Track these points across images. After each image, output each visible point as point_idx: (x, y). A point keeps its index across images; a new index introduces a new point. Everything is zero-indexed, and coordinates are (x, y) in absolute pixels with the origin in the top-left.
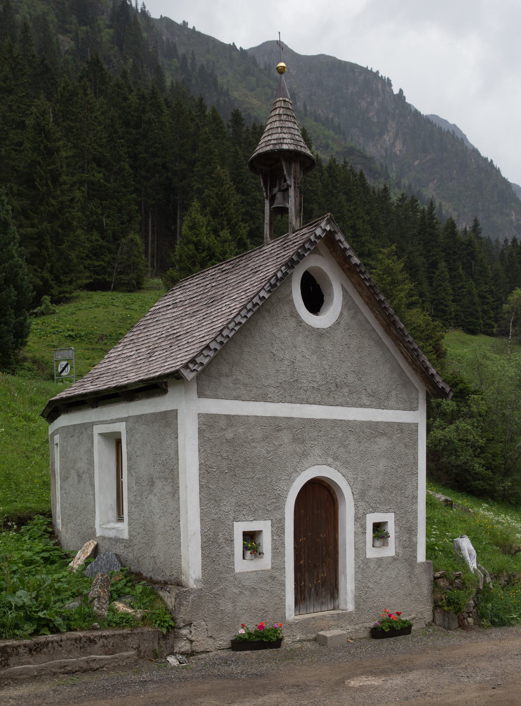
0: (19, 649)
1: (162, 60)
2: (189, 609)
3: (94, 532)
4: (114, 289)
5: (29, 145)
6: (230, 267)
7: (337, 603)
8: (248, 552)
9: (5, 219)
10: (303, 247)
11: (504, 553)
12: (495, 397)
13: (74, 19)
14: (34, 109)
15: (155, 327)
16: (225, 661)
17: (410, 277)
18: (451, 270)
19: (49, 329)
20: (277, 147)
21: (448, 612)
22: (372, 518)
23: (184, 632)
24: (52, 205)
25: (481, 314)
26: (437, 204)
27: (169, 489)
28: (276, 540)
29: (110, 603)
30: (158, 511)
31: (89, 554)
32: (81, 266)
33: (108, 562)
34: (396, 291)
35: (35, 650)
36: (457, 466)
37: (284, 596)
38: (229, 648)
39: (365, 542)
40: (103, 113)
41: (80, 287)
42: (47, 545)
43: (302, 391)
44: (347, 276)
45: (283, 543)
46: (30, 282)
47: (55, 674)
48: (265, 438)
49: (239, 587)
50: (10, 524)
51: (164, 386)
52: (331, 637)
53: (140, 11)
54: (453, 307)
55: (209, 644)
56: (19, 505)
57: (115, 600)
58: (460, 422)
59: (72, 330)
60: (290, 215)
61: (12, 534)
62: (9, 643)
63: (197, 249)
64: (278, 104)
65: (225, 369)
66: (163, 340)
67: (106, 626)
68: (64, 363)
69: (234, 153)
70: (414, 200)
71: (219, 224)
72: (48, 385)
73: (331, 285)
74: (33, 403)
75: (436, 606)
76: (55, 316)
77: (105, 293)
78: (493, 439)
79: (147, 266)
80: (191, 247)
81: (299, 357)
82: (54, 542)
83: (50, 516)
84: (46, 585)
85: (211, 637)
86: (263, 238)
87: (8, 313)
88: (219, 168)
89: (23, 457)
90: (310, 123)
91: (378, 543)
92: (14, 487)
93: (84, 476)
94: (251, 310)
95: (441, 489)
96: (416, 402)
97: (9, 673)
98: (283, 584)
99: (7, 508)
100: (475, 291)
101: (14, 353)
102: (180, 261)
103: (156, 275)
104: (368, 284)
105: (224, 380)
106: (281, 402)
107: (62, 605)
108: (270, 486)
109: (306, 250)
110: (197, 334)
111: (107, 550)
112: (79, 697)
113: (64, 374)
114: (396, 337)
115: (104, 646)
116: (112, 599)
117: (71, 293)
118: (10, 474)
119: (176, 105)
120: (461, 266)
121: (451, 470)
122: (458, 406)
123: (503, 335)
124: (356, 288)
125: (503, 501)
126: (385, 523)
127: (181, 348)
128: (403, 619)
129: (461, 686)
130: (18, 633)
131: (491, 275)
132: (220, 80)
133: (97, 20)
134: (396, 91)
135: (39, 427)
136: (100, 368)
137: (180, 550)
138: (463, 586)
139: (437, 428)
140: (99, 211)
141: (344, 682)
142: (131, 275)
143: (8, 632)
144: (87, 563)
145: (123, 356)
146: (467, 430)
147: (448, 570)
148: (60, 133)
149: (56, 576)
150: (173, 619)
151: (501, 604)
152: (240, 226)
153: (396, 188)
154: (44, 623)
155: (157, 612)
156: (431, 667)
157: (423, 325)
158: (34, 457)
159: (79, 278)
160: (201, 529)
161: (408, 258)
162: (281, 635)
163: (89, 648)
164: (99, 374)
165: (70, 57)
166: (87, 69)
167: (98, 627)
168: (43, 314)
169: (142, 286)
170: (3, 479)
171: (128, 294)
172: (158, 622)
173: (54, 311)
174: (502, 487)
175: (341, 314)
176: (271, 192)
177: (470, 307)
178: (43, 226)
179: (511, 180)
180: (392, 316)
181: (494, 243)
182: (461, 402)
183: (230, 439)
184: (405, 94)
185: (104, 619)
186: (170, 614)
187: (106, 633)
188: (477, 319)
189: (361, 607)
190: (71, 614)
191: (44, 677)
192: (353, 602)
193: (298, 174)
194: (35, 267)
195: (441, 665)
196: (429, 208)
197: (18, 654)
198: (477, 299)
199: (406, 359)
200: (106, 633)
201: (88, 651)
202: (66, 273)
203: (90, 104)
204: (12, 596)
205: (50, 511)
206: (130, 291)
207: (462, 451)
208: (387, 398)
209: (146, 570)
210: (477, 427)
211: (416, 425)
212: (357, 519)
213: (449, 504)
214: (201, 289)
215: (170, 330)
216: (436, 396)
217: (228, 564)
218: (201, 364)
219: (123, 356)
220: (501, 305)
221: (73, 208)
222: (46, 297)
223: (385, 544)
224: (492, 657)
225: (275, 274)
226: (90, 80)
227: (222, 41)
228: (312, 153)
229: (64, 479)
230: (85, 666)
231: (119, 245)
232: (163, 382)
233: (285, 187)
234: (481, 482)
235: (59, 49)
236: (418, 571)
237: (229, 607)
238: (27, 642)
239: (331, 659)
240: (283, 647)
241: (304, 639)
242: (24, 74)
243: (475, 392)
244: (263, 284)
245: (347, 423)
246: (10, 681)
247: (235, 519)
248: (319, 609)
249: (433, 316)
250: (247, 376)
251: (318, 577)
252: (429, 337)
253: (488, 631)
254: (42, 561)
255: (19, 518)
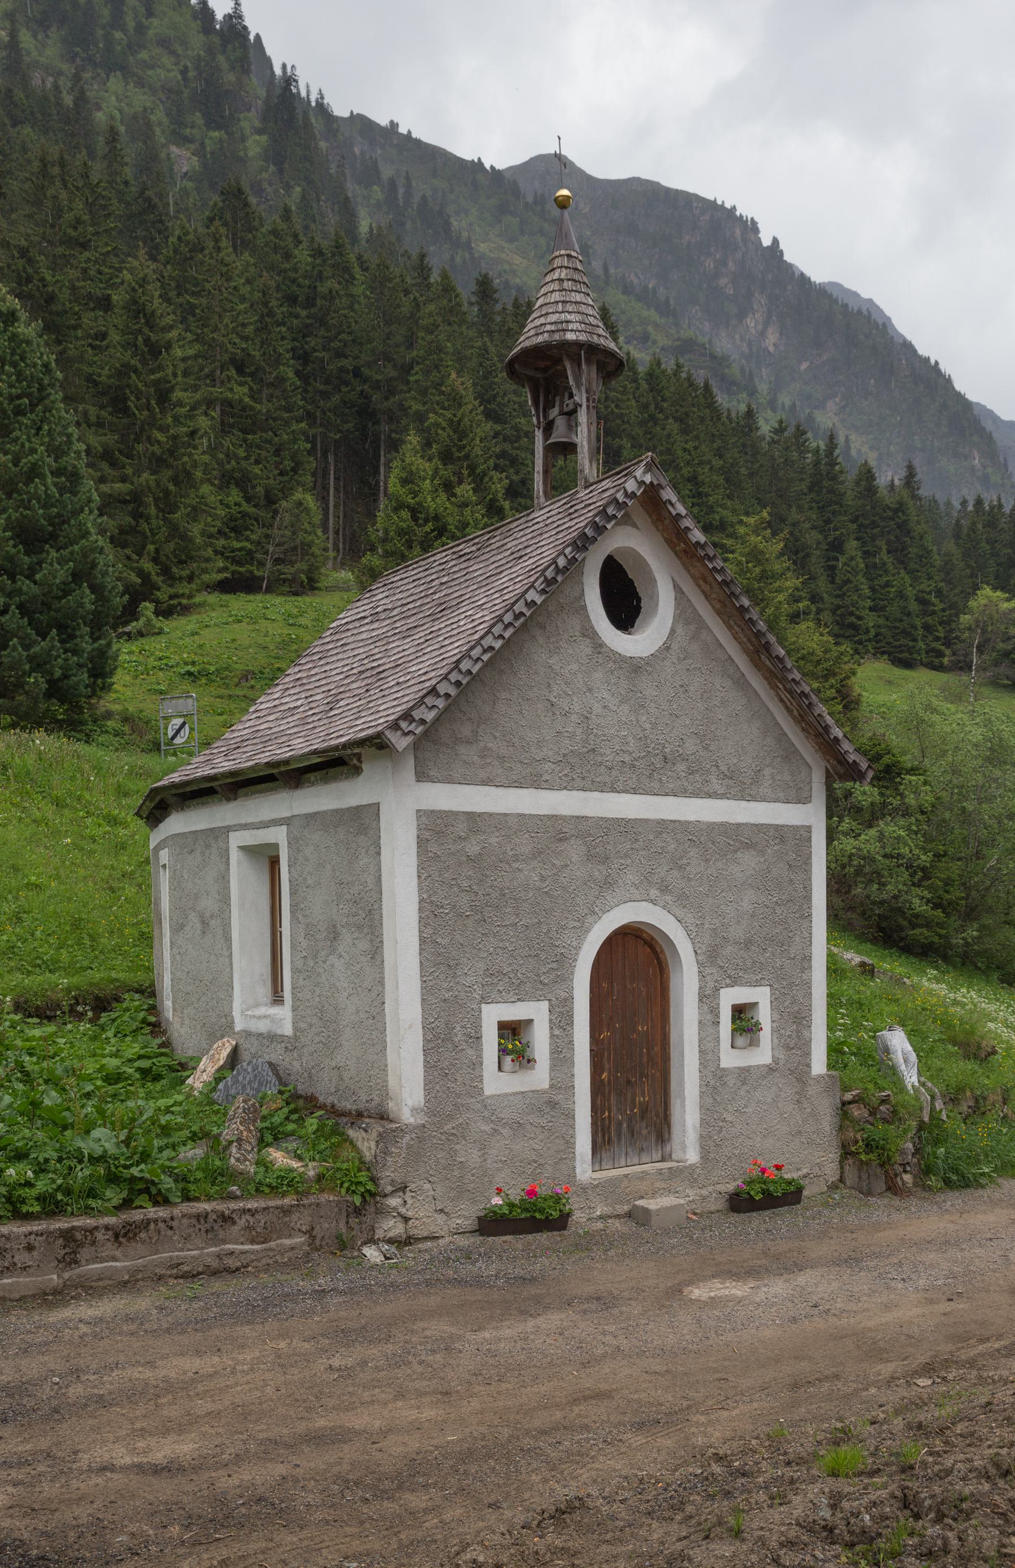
0: (96, 1234)
1: (352, 188)
2: (401, 1162)
3: (231, 1024)
4: (269, 590)
5: (118, 338)
6: (474, 548)
7: (668, 1149)
8: (509, 1058)
9: (75, 467)
10: (603, 512)
11: (967, 1057)
12: (948, 778)
13: (198, 118)
14: (126, 275)
15: (340, 656)
16: (468, 1255)
17: (793, 567)
18: (867, 554)
19: (152, 662)
20: (557, 337)
21: (867, 1163)
22: (730, 997)
23: (394, 1202)
24: (158, 442)
25: (921, 632)
26: (841, 439)
27: (364, 945)
28: (558, 1036)
29: (260, 1151)
30: (346, 985)
31: (221, 1062)
32: (210, 550)
33: (255, 1076)
34: (770, 592)
35: (125, 1235)
36: (882, 902)
37: (573, 1136)
38: (474, 1232)
39: (717, 1039)
40: (248, 281)
41: (208, 586)
42: (146, 1047)
43: (603, 769)
44: (683, 564)
45: (571, 1042)
46: (118, 579)
47: (160, 1278)
48: (536, 854)
49: (492, 1121)
50: (80, 1009)
51: (355, 761)
52: (658, 1210)
53: (313, 104)
54: (871, 620)
55: (438, 1224)
56: (97, 976)
57: (268, 1145)
58: (887, 824)
59: (193, 663)
60: (579, 457)
61: (84, 1026)
62: (78, 1222)
63: (415, 518)
64: (557, 262)
65: (466, 731)
66: (353, 678)
67: (253, 1192)
68: (178, 722)
69: (479, 348)
70: (800, 432)
71: (454, 474)
72: (149, 761)
73: (653, 581)
74: (122, 792)
75: (846, 1153)
76: (163, 639)
77: (251, 597)
78: (945, 855)
79: (326, 550)
80: (405, 514)
81: (597, 708)
82: (159, 1041)
83: (153, 994)
84: (144, 1118)
85: (441, 1211)
86: (532, 498)
87: (78, 633)
88: (453, 375)
89: (104, 889)
90: (615, 297)
91: (740, 1041)
92: (87, 942)
93: (213, 923)
94: (510, 624)
95: (853, 944)
96: (807, 788)
97: (79, 1276)
98: (570, 1116)
99: (75, 980)
100: (910, 592)
101: (89, 704)
102: (385, 540)
103: (343, 564)
104: (720, 579)
105: (462, 749)
106: (565, 788)
107: (173, 1154)
108: (547, 940)
109: (610, 518)
110: (414, 669)
111: (254, 1056)
112: (204, 1320)
113: (178, 741)
114: (771, 672)
115: (248, 1228)
116: (262, 1143)
117: (190, 597)
118: (80, 919)
119: (378, 266)
120: (884, 548)
121: (871, 909)
122: (881, 794)
123: (961, 669)
124: (699, 586)
125: (963, 964)
126: (754, 1005)
127: (386, 692)
128: (787, 1176)
129: (892, 1296)
130: (94, 1205)
131: (938, 563)
132: (455, 223)
133: (239, 120)
134: (767, 242)
135: (133, 836)
136: (241, 730)
137: (385, 1055)
138: (894, 1117)
139: (846, 834)
140: (241, 453)
141: (681, 1291)
142: (298, 565)
143: (77, 1202)
144: (218, 1080)
145: (282, 708)
146: (899, 838)
147: (866, 1089)
148: (172, 317)
149: (162, 1103)
150: (373, 1180)
151: (961, 1148)
152: (491, 478)
153: (769, 411)
154: (141, 1186)
155: (345, 1166)
156: (838, 1262)
157: (819, 652)
158: (124, 888)
159: (205, 571)
160: (423, 1016)
161: (791, 533)
162: (568, 1207)
163: (221, 1232)
164: (239, 739)
165: (190, 185)
166: (221, 204)
167: (238, 1193)
168: (141, 634)
169: (318, 585)
170: (68, 929)
171: (293, 598)
172: (346, 1185)
173: (161, 629)
174: (963, 939)
175: (673, 631)
176: (545, 416)
177: (901, 620)
178: (141, 479)
179: (972, 396)
180: (764, 634)
181: (942, 507)
182: (887, 788)
183: (475, 856)
184: (782, 246)
185: (250, 1180)
186: (368, 1169)
187: (252, 1205)
188: (915, 640)
189: (712, 1155)
190: (189, 1171)
191: (141, 1283)
192: (698, 1148)
193: (594, 384)
194: (128, 551)
195: (856, 1260)
196: (827, 446)
197: (93, 1243)
198: (914, 606)
199: (790, 711)
200: (252, 1205)
201: (221, 1236)
202: (181, 562)
203: (226, 265)
204: (83, 1139)
205: (152, 985)
206: (296, 594)
207: (891, 876)
208: (756, 781)
209: (325, 1090)
210: (916, 833)
211: (808, 829)
212: (702, 997)
213: (867, 970)
214: (422, 588)
215: (365, 661)
216: (843, 778)
217: (472, 1080)
218: (423, 722)
219: (282, 708)
220: (957, 615)
221: (195, 448)
222: (147, 604)
223: (754, 1043)
224: (946, 1243)
225: (554, 562)
226: (225, 224)
227: (458, 155)
228: (620, 349)
229: (178, 928)
230: (215, 1264)
231: (276, 512)
232: (355, 755)
233: (571, 407)
234: (924, 931)
235: (172, 169)
236: (812, 1091)
237: (474, 1157)
238: (111, 1220)
239: (658, 1249)
240: (572, 1228)
241: (609, 1213)
242: (109, 214)
243: (912, 771)
244: (532, 579)
245: (683, 826)
246: (80, 1290)
247: (484, 1000)
248: (636, 1160)
249: (836, 636)
250: (504, 743)
251: (633, 1102)
252: (829, 674)
253: (940, 1197)
254: (138, 1076)
255: (97, 998)
